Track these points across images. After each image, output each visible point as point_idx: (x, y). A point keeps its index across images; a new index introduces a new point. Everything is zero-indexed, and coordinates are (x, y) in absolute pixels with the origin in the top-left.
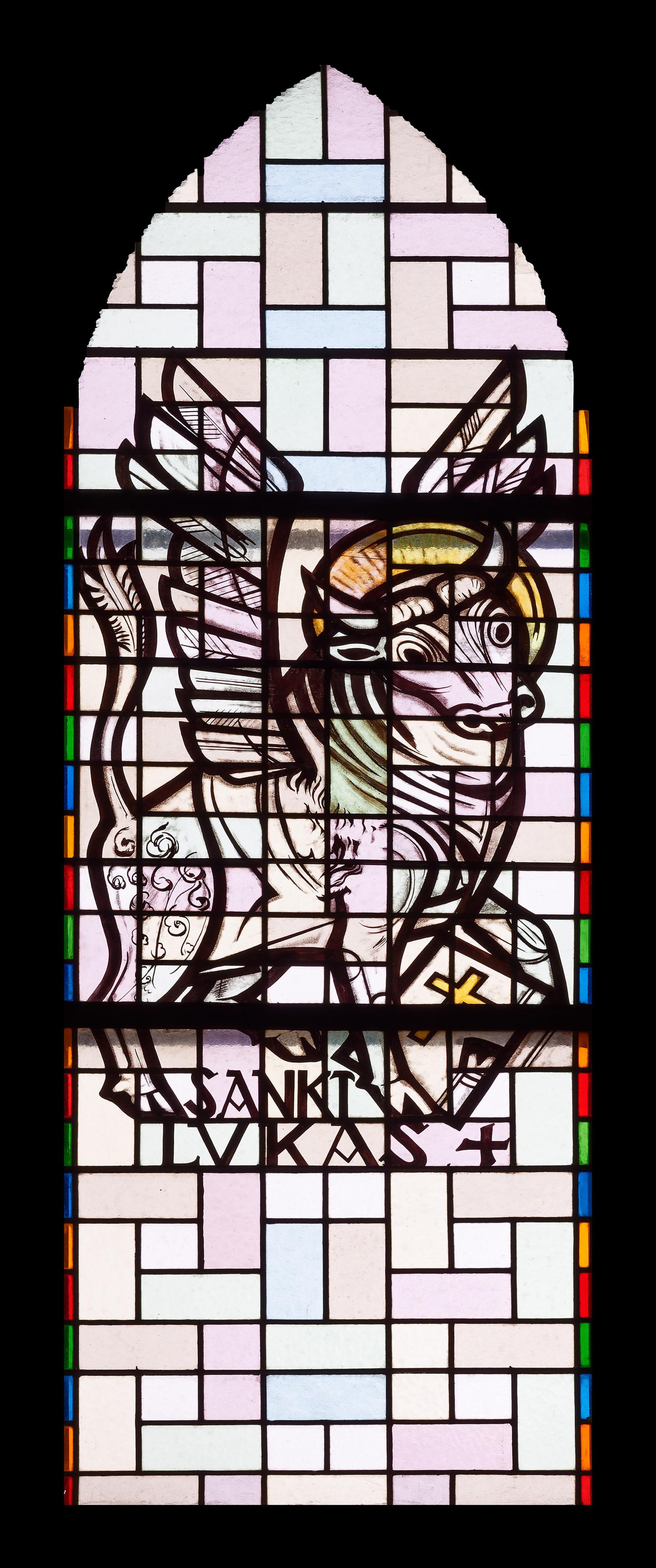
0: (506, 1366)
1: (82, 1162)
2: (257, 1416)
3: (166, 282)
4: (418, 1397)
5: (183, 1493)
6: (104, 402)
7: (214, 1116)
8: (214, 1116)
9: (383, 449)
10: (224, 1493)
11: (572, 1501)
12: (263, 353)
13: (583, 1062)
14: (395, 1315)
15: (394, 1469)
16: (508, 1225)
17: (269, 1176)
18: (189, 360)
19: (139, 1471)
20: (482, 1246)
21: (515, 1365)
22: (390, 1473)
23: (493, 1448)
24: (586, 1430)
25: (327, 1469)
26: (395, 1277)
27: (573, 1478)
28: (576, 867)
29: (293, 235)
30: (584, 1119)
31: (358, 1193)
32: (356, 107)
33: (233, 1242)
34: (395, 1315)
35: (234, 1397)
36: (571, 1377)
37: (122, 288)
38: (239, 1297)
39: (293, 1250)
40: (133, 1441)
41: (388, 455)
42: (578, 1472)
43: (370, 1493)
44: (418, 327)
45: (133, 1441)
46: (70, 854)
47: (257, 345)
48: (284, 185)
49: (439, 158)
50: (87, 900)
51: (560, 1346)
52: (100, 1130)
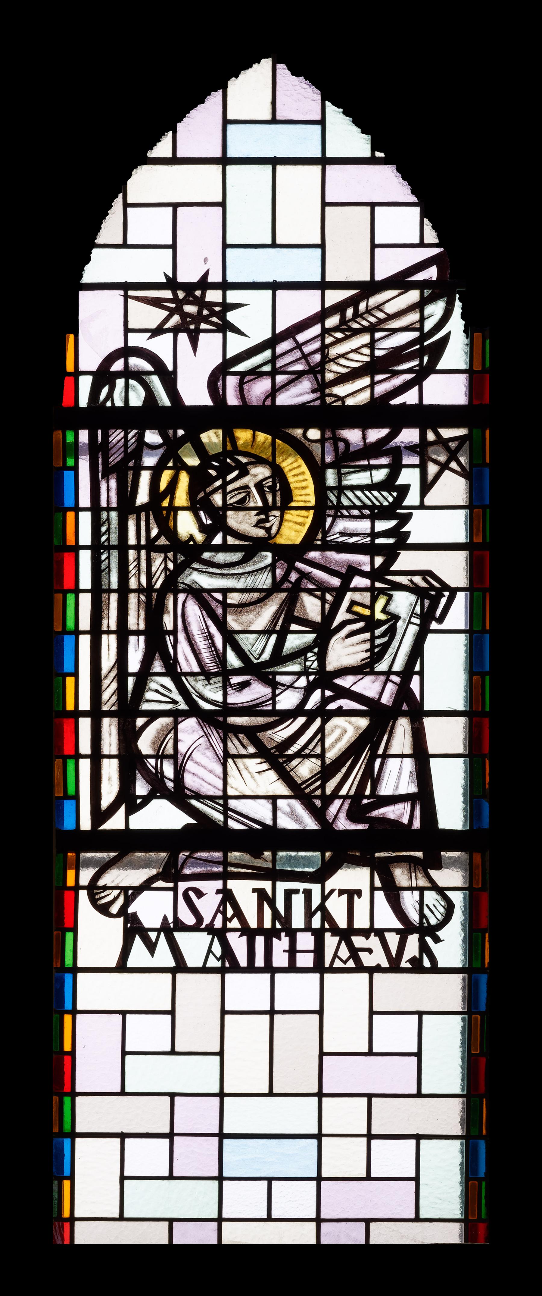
2: (315, 1174)
3: (149, 226)
4: (343, 1157)
5: (156, 1235)
6: (99, 326)
7: (203, 926)
8: (203, 926)
10: (186, 1235)
12: (224, 161)
14: (323, 1216)
15: (224, 1216)
16: (375, 1017)
17: (179, 976)
19: (417, 1219)
20: (396, 1034)
22: (318, 1220)
23: (398, 1201)
26: (325, 1058)
29: (248, 183)
31: (297, 990)
33: (197, 1029)
35: (197, 1156)
37: (110, 230)
39: (247, 1036)
40: (112, 1195)
43: (304, 1235)
45: (112, 1195)
46: (70, 707)
48: (241, 142)
51: (450, 1116)
52: (95, 936)
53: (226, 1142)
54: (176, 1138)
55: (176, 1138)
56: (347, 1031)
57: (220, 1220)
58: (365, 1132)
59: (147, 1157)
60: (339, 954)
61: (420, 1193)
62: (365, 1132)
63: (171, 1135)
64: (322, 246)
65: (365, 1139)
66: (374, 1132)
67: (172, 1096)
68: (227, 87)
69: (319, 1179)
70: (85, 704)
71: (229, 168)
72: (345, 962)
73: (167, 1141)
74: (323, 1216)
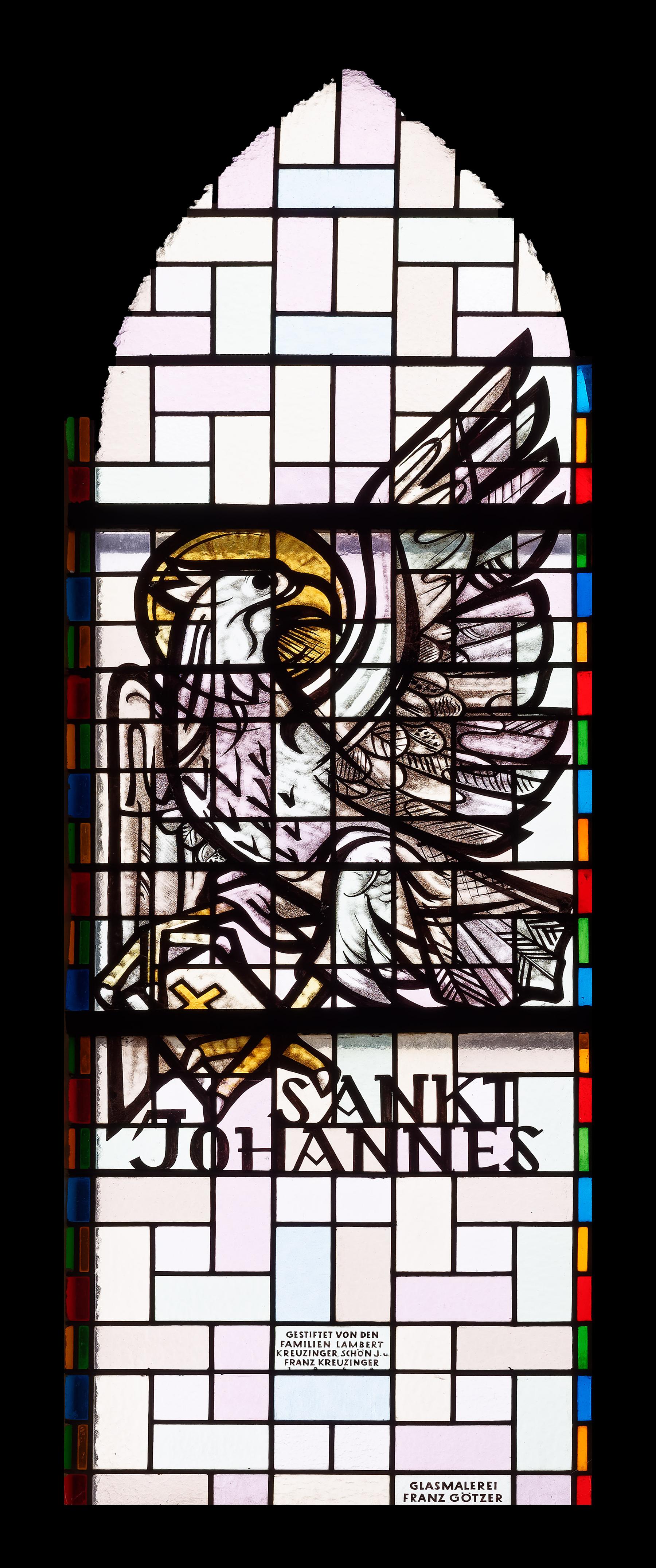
0: (505, 1367)
1: (266, 502)
4: (422, 1398)
5: (190, 1493)
10: (233, 1493)
11: (567, 1501)
12: (275, 213)
13: (585, 1067)
14: (398, 1467)
16: (459, 1229)
18: (482, 368)
20: (484, 1249)
21: (515, 1367)
24: (583, 1432)
27: (571, 1080)
29: (304, 239)
30: (584, 1125)
31: (363, 1197)
33: (243, 1244)
34: (398, 1319)
35: (242, 1397)
36: (569, 1379)
38: (251, 1300)
39: (303, 1252)
42: (574, 1473)
44: (424, 334)
49: (449, 157)
51: (559, 1348)
56: (423, 1245)
57: (271, 1472)
58: (449, 1368)
60: (308, 1152)
61: (528, 1442)
62: (449, 1368)
64: (334, 312)
66: (459, 1367)
67: (211, 1421)
68: (280, 124)
69: (271, 1422)
70: (103, 858)
71: (282, 221)
72: (316, 1163)
74: (398, 1467)
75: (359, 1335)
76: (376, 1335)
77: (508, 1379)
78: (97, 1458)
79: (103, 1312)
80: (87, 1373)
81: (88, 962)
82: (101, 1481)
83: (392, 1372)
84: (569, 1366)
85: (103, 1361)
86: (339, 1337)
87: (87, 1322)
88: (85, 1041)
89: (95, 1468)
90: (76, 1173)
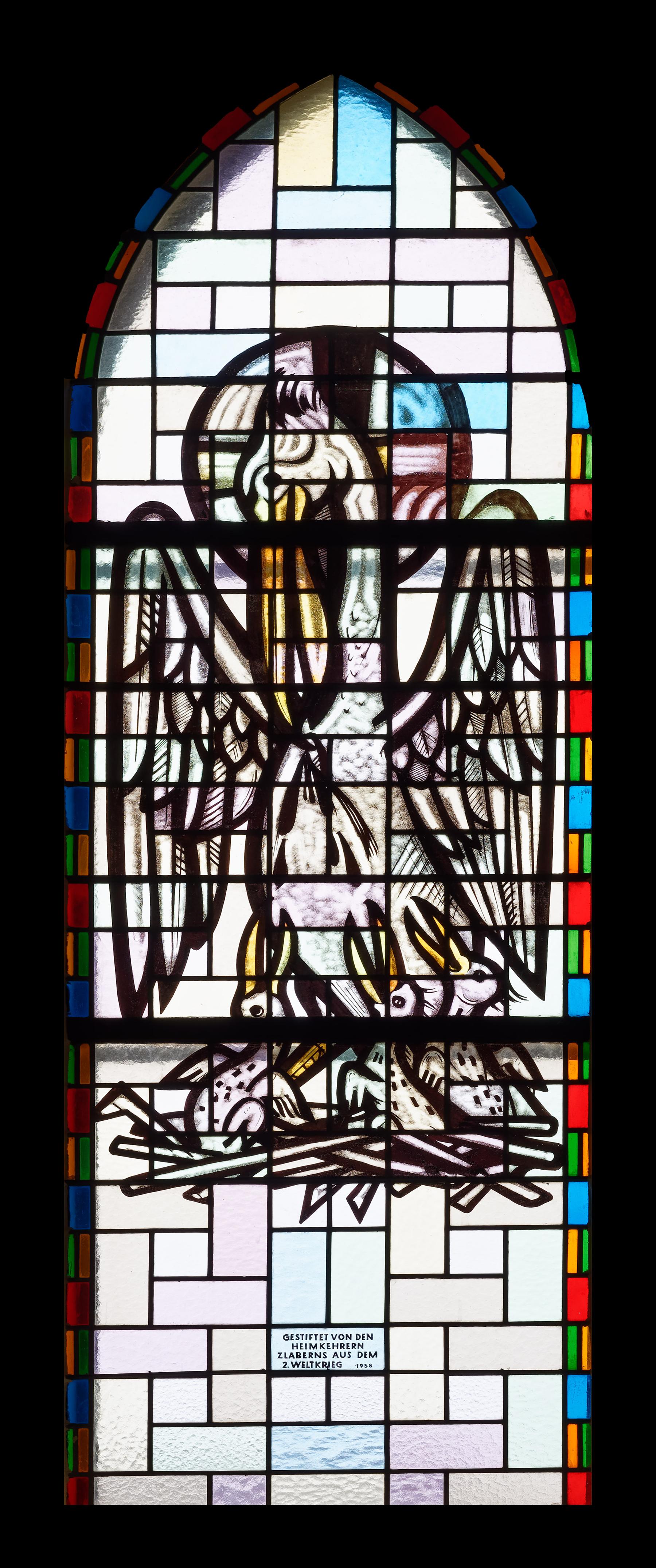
4: (416, 1397)
5: (192, 1494)
9: (324, 1234)
11: (558, 1500)
12: (274, 234)
14: (393, 1319)
15: (273, 1469)
23: (485, 1447)
25: (327, 1469)
27: (559, 1476)
28: (568, 377)
32: (363, 122)
33: (240, 1250)
35: (240, 1397)
36: (559, 1378)
38: (247, 1303)
41: (329, 1229)
47: (268, 227)
50: (103, 915)
53: (451, 1378)
54: (215, 1377)
55: (215, 1377)
59: (181, 1400)
60: (301, 383)
63: (208, 1374)
65: (442, 1376)
66: (452, 1367)
67: (210, 1328)
69: (269, 1424)
73: (381, 1379)
74: (393, 1319)
75: (354, 1337)
76: (370, 1337)
77: (500, 1378)
78: (98, 1290)
79: (103, 1316)
80: (88, 1377)
81: (87, 975)
82: (102, 1483)
83: (386, 1373)
84: (559, 1366)
85: (103, 1365)
86: (334, 1339)
87: (87, 1326)
88: (84, 1050)
89: (96, 1372)
90: (76, 1376)
